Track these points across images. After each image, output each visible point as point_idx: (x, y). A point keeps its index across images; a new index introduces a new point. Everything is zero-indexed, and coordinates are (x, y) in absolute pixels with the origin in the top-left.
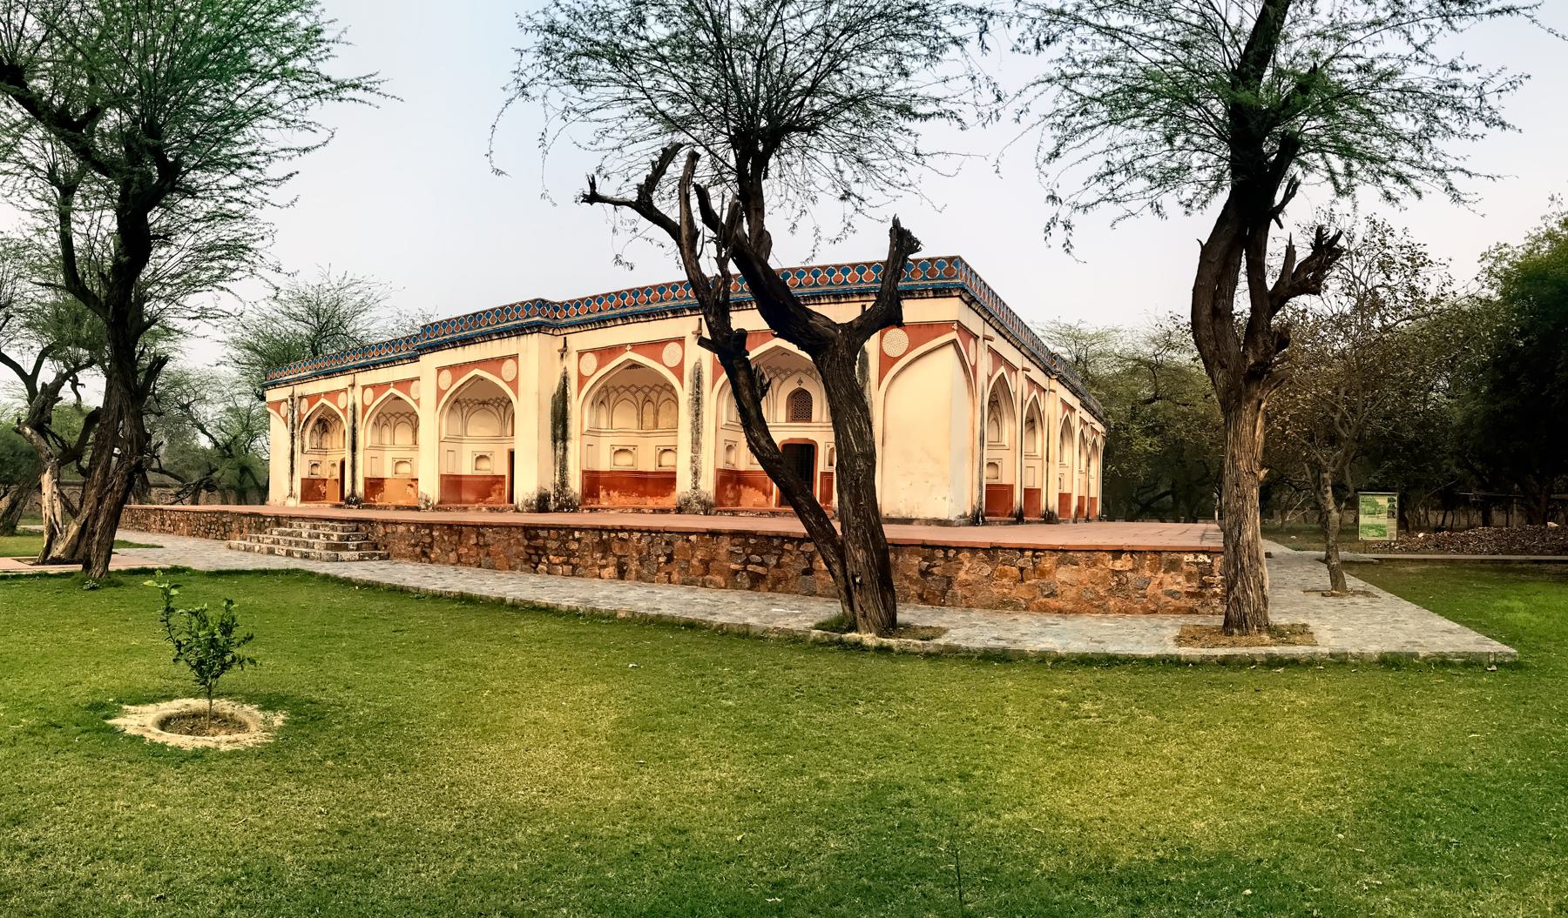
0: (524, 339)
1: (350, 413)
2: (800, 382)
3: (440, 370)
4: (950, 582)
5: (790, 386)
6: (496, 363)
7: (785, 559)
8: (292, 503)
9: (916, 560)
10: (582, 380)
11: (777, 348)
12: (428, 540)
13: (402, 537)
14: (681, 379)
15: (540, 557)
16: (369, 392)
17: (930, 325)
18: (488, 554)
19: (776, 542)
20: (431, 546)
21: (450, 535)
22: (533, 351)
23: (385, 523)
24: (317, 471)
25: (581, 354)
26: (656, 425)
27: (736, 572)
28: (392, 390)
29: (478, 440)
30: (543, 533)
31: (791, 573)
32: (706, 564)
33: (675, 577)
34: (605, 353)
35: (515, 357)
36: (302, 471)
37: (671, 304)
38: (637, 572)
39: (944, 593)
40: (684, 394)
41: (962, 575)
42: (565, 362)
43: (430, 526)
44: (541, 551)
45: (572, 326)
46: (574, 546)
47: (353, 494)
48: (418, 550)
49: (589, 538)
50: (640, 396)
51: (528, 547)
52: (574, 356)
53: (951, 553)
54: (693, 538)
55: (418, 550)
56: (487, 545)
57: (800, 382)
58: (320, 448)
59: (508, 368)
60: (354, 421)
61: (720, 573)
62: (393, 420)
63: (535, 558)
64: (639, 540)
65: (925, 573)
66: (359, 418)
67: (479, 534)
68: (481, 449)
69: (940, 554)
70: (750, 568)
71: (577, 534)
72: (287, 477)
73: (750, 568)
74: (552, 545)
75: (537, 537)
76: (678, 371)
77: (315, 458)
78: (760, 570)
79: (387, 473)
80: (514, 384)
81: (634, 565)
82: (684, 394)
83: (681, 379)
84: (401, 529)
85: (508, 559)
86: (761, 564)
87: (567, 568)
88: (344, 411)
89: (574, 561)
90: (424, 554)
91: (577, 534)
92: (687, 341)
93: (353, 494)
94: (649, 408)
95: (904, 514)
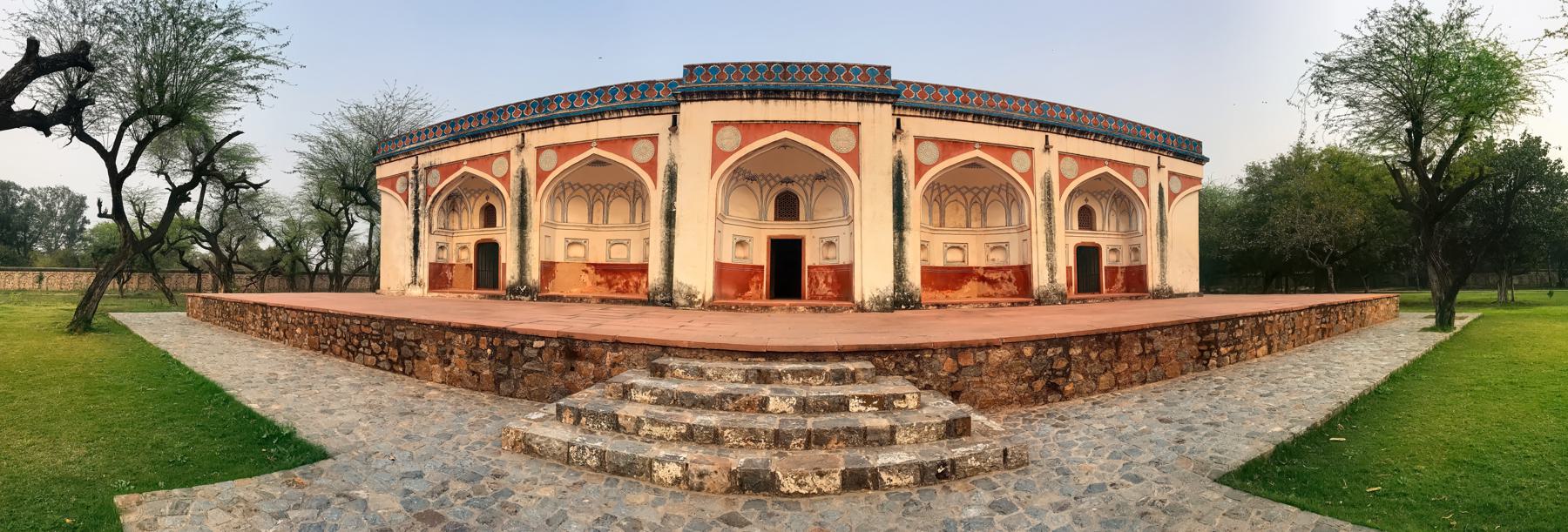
0: (868, 107)
1: (514, 183)
3: (718, 125)
5: (482, 202)
6: (823, 129)
8: (416, 291)
10: (920, 169)
12: (1063, 364)
13: (1002, 368)
18: (1157, 363)
21: (1100, 350)
22: (876, 118)
23: (956, 350)
24: (444, 254)
26: (942, 224)
28: (594, 151)
29: (740, 222)
30: (1214, 327)
34: (949, 146)
35: (855, 127)
36: (428, 255)
40: (1036, 199)
43: (1065, 341)
44: (1212, 345)
45: (913, 108)
47: (522, 281)
48: (1039, 384)
49: (1250, 324)
50: (969, 196)
51: (1199, 344)
55: (1039, 384)
56: (1154, 352)
58: (446, 228)
59: (842, 138)
60: (523, 190)
66: (532, 188)
67: (1144, 340)
68: (743, 232)
72: (409, 262)
74: (1222, 336)
75: (1209, 331)
76: (1029, 176)
77: (442, 239)
79: (559, 257)
80: (853, 158)
82: (1036, 199)
84: (997, 356)
85: (1181, 362)
87: (1233, 356)
88: (505, 179)
89: (1238, 348)
90: (1053, 388)
93: (522, 281)
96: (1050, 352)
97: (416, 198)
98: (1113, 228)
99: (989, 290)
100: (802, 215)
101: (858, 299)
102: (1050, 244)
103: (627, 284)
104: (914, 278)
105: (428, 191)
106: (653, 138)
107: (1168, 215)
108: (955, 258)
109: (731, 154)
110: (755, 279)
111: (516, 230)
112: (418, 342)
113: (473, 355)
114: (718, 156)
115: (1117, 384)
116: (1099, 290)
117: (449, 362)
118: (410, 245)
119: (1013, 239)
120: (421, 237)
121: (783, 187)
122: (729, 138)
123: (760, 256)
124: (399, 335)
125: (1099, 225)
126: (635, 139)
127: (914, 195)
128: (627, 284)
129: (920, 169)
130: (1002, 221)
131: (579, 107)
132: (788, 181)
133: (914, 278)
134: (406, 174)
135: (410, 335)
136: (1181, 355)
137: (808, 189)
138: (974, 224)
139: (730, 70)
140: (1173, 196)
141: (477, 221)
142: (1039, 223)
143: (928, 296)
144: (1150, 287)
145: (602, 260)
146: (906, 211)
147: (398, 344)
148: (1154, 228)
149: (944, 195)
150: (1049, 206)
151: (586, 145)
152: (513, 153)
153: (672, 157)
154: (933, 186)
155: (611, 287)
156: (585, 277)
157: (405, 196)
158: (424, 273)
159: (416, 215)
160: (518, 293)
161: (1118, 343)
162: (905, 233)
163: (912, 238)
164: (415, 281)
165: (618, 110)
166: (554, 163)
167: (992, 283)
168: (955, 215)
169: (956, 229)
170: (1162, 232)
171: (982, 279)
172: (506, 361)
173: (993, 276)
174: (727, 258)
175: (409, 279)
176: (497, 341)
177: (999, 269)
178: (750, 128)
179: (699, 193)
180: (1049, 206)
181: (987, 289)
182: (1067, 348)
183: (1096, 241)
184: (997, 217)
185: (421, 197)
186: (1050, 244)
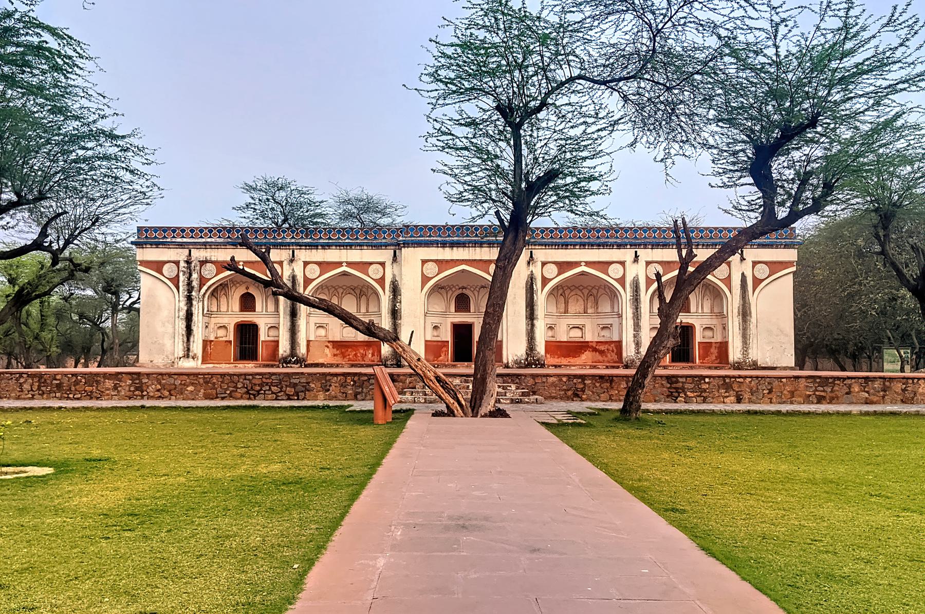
2: (247, 288)
3: (424, 262)
4: (915, 394)
5: (242, 291)
7: (836, 388)
9: (900, 385)
10: (545, 281)
11: (463, 271)
14: (624, 287)
15: (679, 393)
16: (317, 269)
17: (447, 261)
19: (830, 380)
20: (583, 391)
21: (601, 383)
25: (544, 264)
26: (566, 311)
27: (810, 396)
30: (680, 380)
31: (839, 394)
32: (792, 393)
33: (774, 400)
34: (563, 266)
37: (619, 241)
38: (749, 399)
39: (913, 398)
40: (626, 296)
41: (920, 390)
42: (531, 268)
43: (583, 377)
46: (705, 386)
48: (570, 393)
49: (715, 382)
50: (586, 292)
52: (540, 264)
53: (916, 381)
54: (784, 380)
55: (570, 393)
57: (247, 288)
61: (800, 396)
62: (341, 291)
63: (676, 394)
64: (750, 382)
65: (904, 390)
69: (911, 381)
70: (817, 393)
71: (707, 380)
73: (817, 393)
75: (677, 382)
76: (622, 281)
78: (822, 394)
79: (312, 338)
81: (747, 396)
82: (626, 296)
83: (624, 287)
84: (551, 379)
85: (654, 396)
86: (824, 391)
91: (707, 380)
92: (627, 264)
94: (364, 299)
95: (770, 365)
96: (575, 381)
97: (189, 284)
98: (707, 309)
99: (600, 358)
100: (472, 309)
101: (505, 361)
102: (637, 326)
103: (356, 355)
104: (541, 349)
105: (203, 281)
106: (383, 264)
107: (752, 299)
108: (576, 334)
109: (432, 278)
110: (444, 349)
111: (288, 318)
112: (308, 383)
113: (343, 385)
114: (425, 279)
115: (610, 399)
116: (693, 361)
117: (329, 390)
118: (182, 325)
119: (614, 321)
120: (195, 318)
121: (460, 291)
122: (431, 269)
123: (447, 335)
124: (296, 381)
125: (693, 308)
126: (371, 263)
127: (541, 298)
128: (356, 355)
129: (545, 281)
130: (608, 309)
131: (335, 238)
132: (463, 288)
133: (541, 349)
134: (177, 263)
135: (303, 380)
136: (654, 392)
137: (476, 293)
138: (590, 311)
139: (430, 229)
140: (757, 282)
141: (236, 305)
142: (628, 312)
143: (550, 360)
144: (731, 359)
145: (338, 338)
146: (535, 307)
147: (295, 385)
148: (736, 311)
149: (567, 292)
150: (636, 300)
151: (339, 264)
152: (285, 264)
153: (394, 276)
154: (551, 293)
155: (344, 357)
156: (327, 351)
157: (175, 281)
158: (197, 347)
159: (189, 299)
160: (290, 362)
161: (611, 381)
162: (535, 322)
163: (540, 326)
164: (187, 354)
165: (361, 245)
166: (318, 273)
167: (602, 352)
168: (575, 306)
169: (577, 315)
170: (745, 313)
171: (595, 350)
172: (361, 386)
173: (602, 348)
174: (429, 338)
175: (181, 354)
176: (356, 378)
177: (606, 343)
178: (442, 264)
179: (413, 299)
180: (636, 300)
181: (598, 356)
182: (583, 380)
183: (690, 321)
184: (605, 307)
185: (195, 284)
186: (637, 326)
